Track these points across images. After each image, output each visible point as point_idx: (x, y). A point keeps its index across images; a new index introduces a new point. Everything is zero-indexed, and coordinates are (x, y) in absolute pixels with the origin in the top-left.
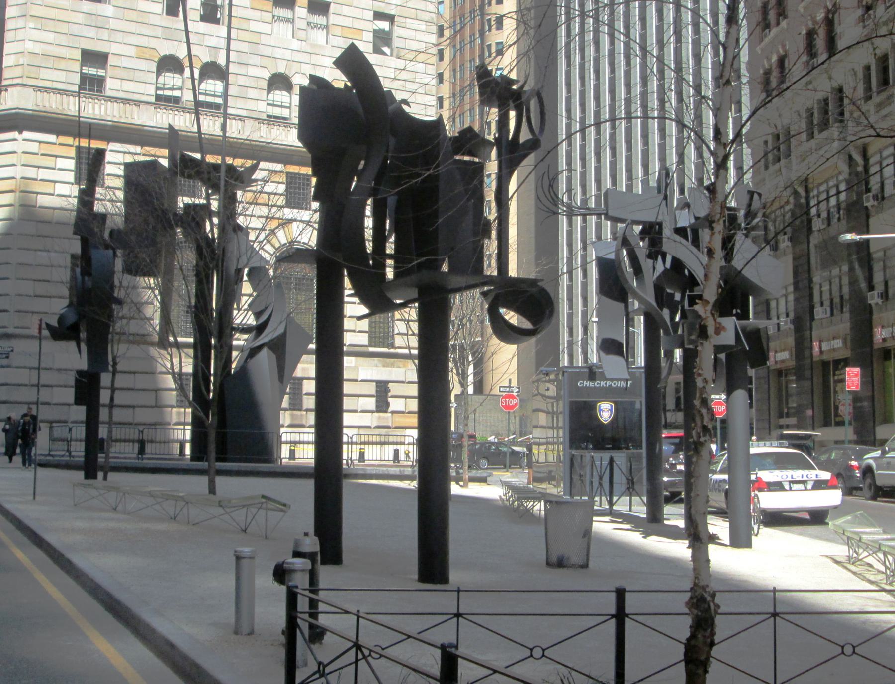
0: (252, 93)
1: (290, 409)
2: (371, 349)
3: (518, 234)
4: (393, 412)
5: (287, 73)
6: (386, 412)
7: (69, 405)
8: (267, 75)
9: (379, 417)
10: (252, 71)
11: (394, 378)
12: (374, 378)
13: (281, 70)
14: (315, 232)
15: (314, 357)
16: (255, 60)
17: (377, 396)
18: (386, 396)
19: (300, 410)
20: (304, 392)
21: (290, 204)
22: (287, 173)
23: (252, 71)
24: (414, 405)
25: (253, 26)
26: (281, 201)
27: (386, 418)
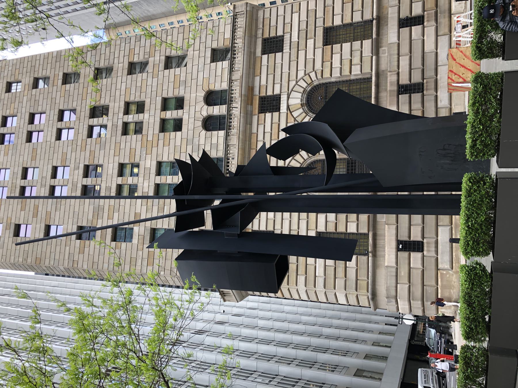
0: (214, 141)
1: (423, 92)
2: (374, 36)
3: (280, 104)
4: (423, 237)
5: (201, 120)
6: (423, 243)
7: (423, 256)
8: (204, 132)
9: (428, 21)
10: (202, 142)
11: (396, 15)
12: (396, 30)
13: (200, 123)
14: (293, 124)
15: (378, 215)
16: (196, 140)
17: (411, 26)
18: (411, 18)
19: (423, 84)
20: (409, 82)
21: (278, 109)
22: (259, 113)
23: (202, 142)
24: (417, 218)
25: (178, 143)
26: (276, 114)
27: (429, 14)
